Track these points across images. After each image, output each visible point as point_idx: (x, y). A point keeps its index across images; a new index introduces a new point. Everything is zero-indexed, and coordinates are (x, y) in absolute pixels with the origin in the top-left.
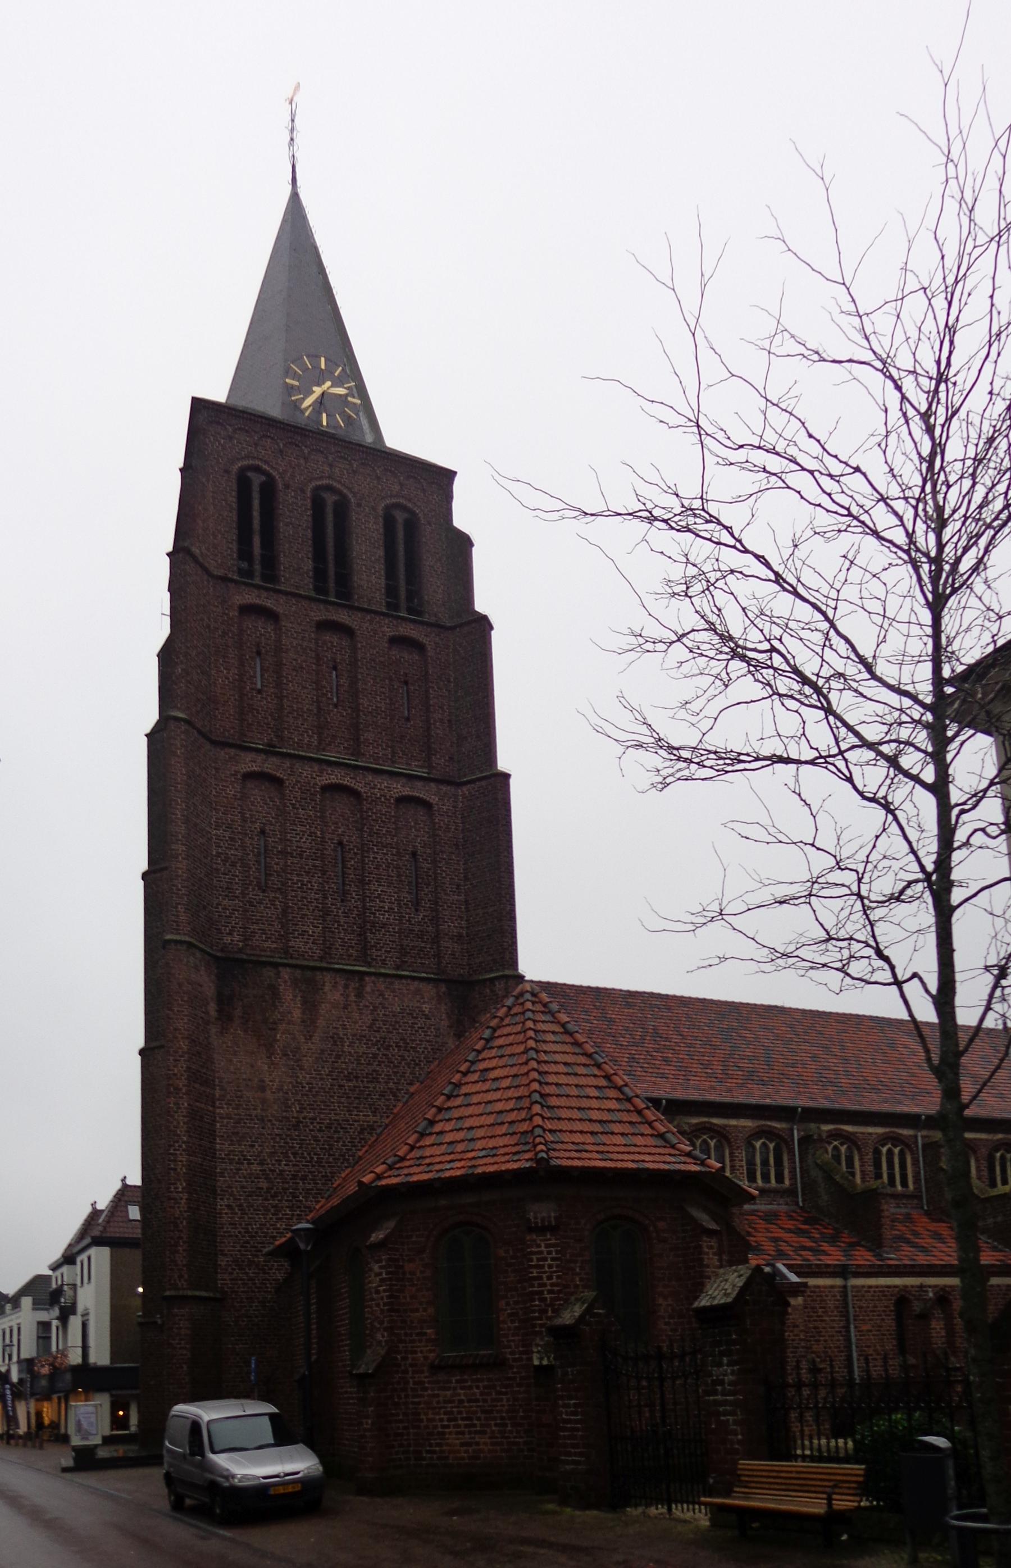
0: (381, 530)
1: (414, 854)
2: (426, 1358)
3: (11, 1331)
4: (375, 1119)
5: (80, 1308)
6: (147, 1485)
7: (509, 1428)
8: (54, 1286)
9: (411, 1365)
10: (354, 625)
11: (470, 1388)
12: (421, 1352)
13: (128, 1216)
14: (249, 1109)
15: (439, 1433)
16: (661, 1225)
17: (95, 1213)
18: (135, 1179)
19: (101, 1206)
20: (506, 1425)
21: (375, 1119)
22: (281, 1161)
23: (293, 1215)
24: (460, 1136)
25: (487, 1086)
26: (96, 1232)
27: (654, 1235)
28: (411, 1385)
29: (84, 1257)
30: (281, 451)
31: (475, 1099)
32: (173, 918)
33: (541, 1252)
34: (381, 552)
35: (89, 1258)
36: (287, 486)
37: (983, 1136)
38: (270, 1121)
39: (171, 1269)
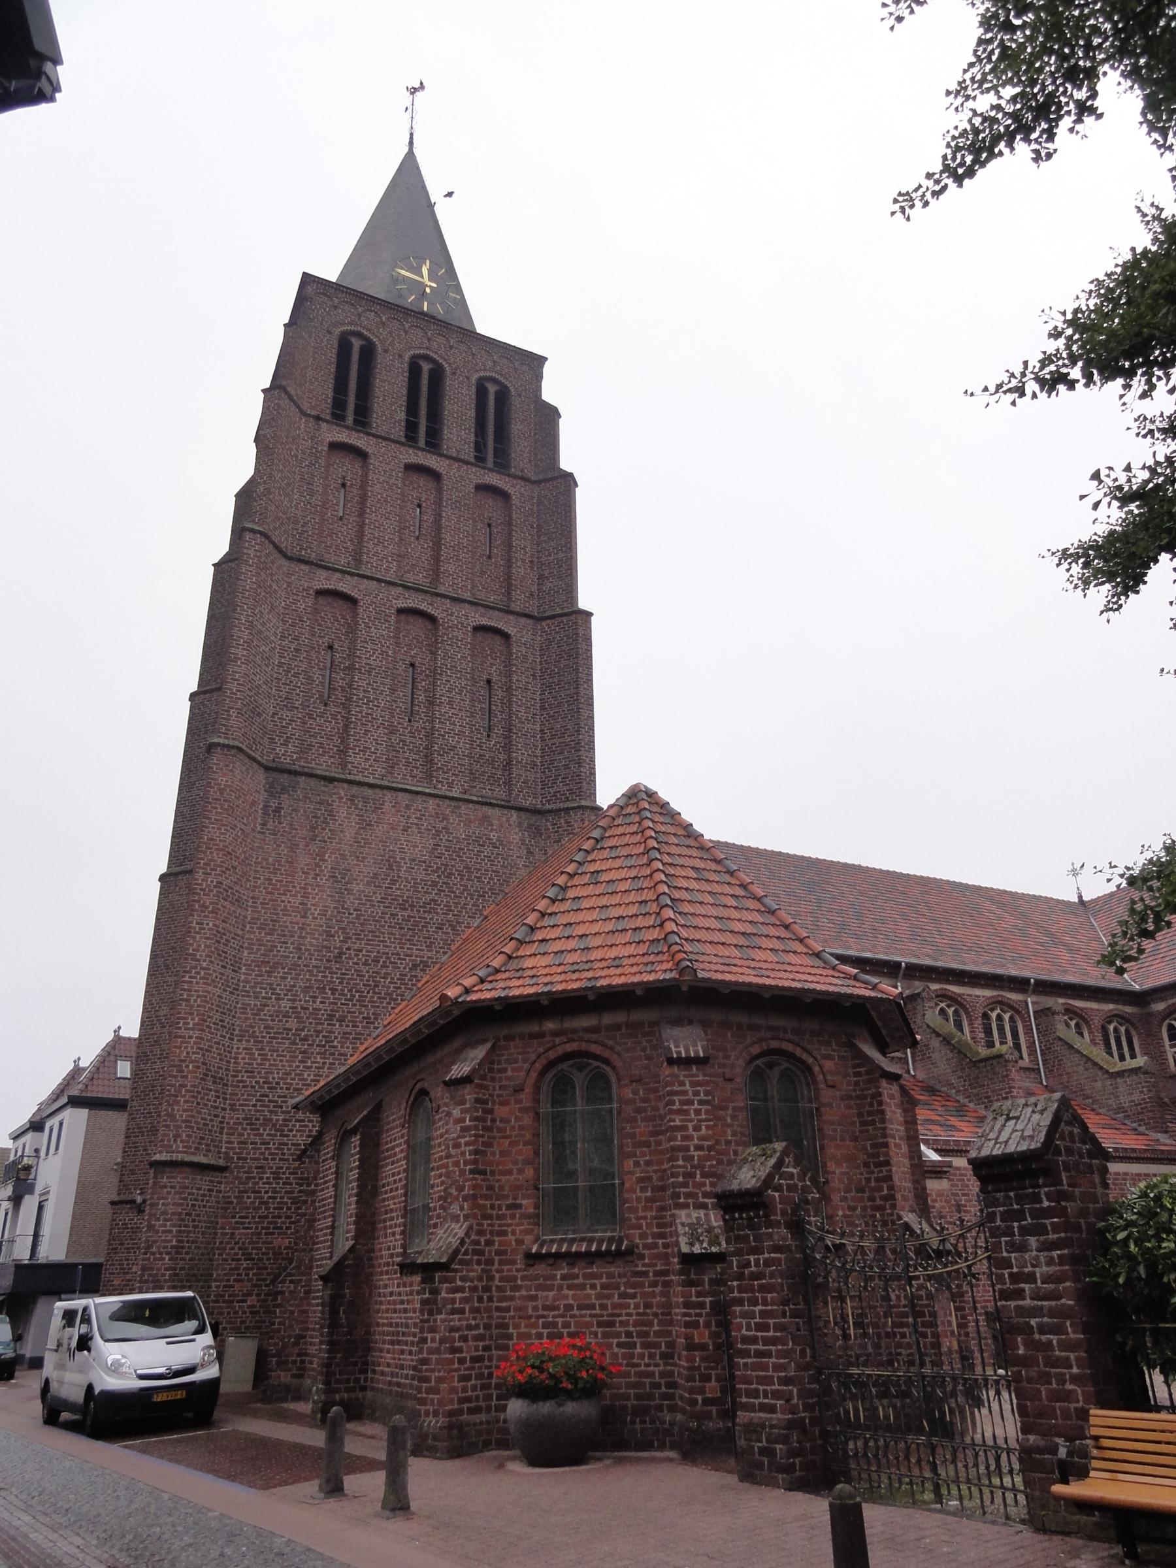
0: (474, 396)
1: (489, 682)
2: (520, 1242)
4: (429, 954)
5: (38, 1189)
7: (639, 1350)
8: (12, 1158)
9: (498, 1253)
10: (441, 470)
11: (582, 1287)
12: (514, 1233)
13: (116, 1073)
14: (285, 936)
16: (828, 1065)
17: (77, 1071)
18: (132, 1030)
19: (82, 1064)
20: (634, 1345)
21: (429, 954)
22: (316, 997)
23: (324, 1063)
24: (572, 944)
25: (601, 889)
26: (75, 1091)
27: (821, 1077)
28: (497, 1282)
29: (54, 1122)
30: (383, 323)
31: (586, 904)
32: (223, 722)
33: (685, 1093)
34: (472, 413)
35: (61, 1124)
37: (1094, 1005)
38: (307, 950)
39: (167, 1126)
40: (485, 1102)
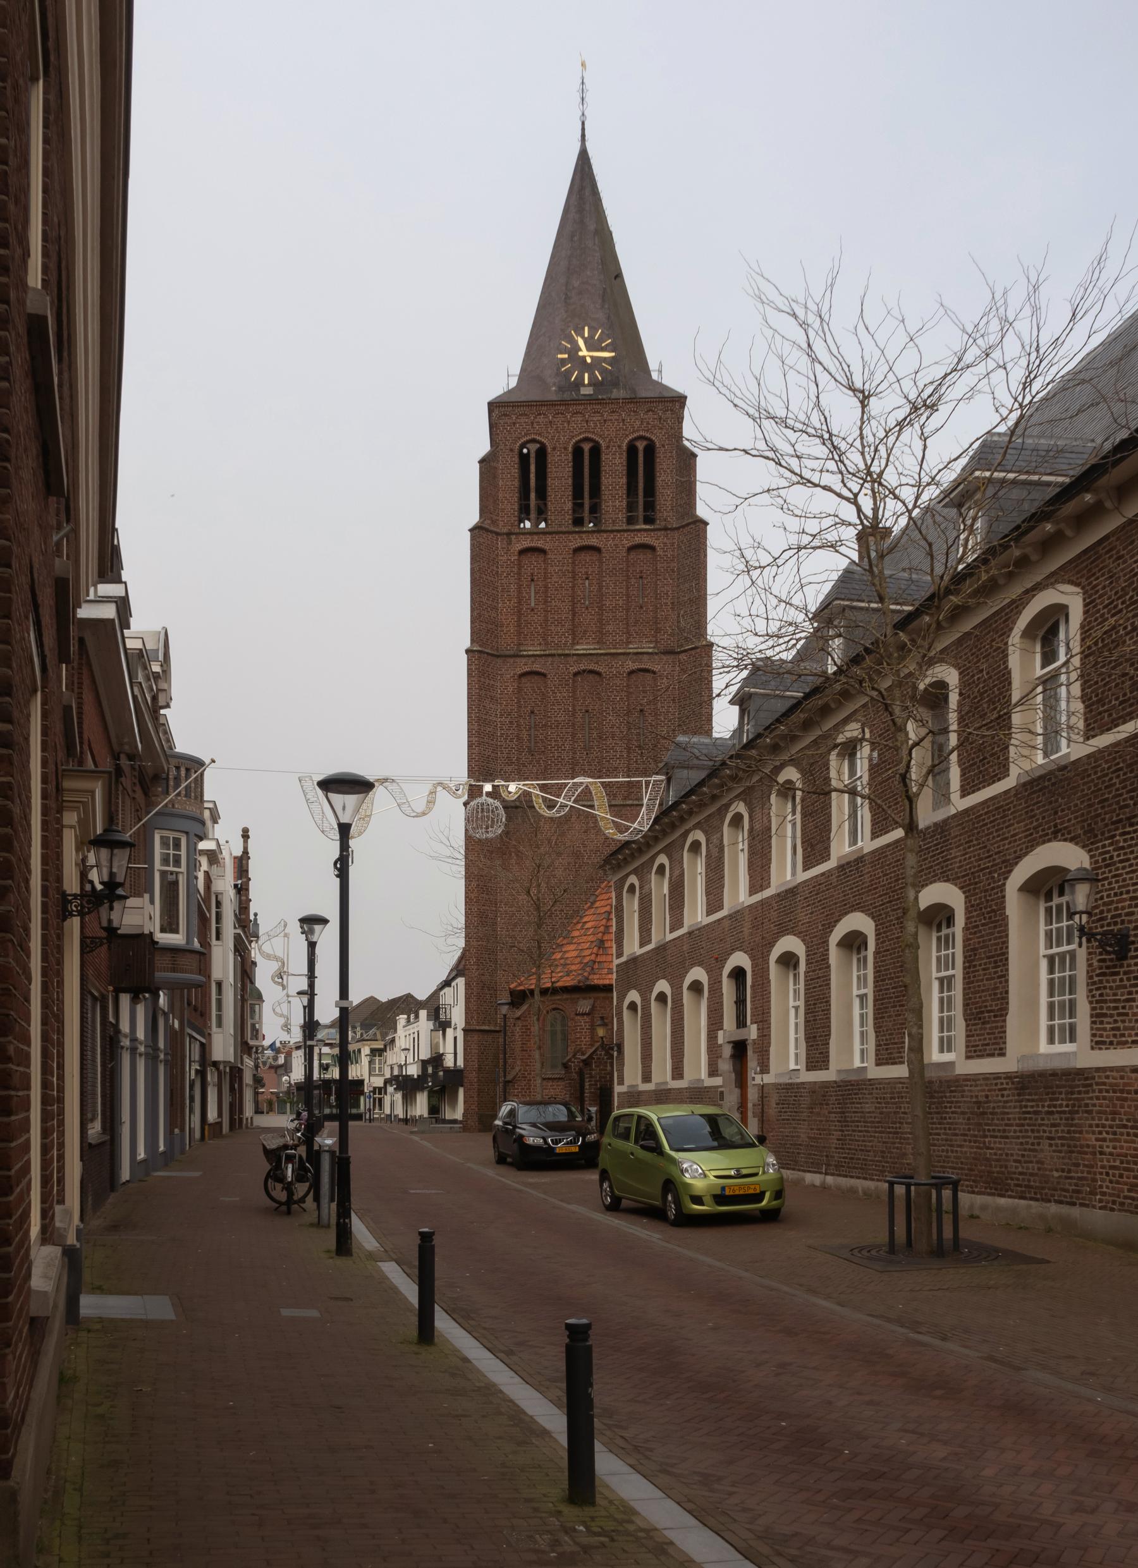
6: (485, 1146)
36: (554, 449)
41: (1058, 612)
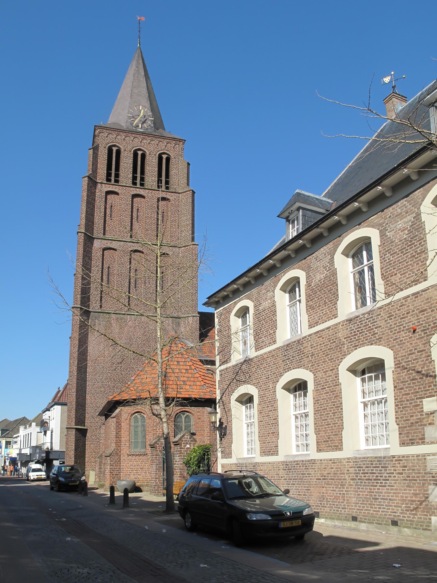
3: (28, 434)
5: (50, 429)
15: (129, 475)
40: (119, 422)
41: (296, 281)
